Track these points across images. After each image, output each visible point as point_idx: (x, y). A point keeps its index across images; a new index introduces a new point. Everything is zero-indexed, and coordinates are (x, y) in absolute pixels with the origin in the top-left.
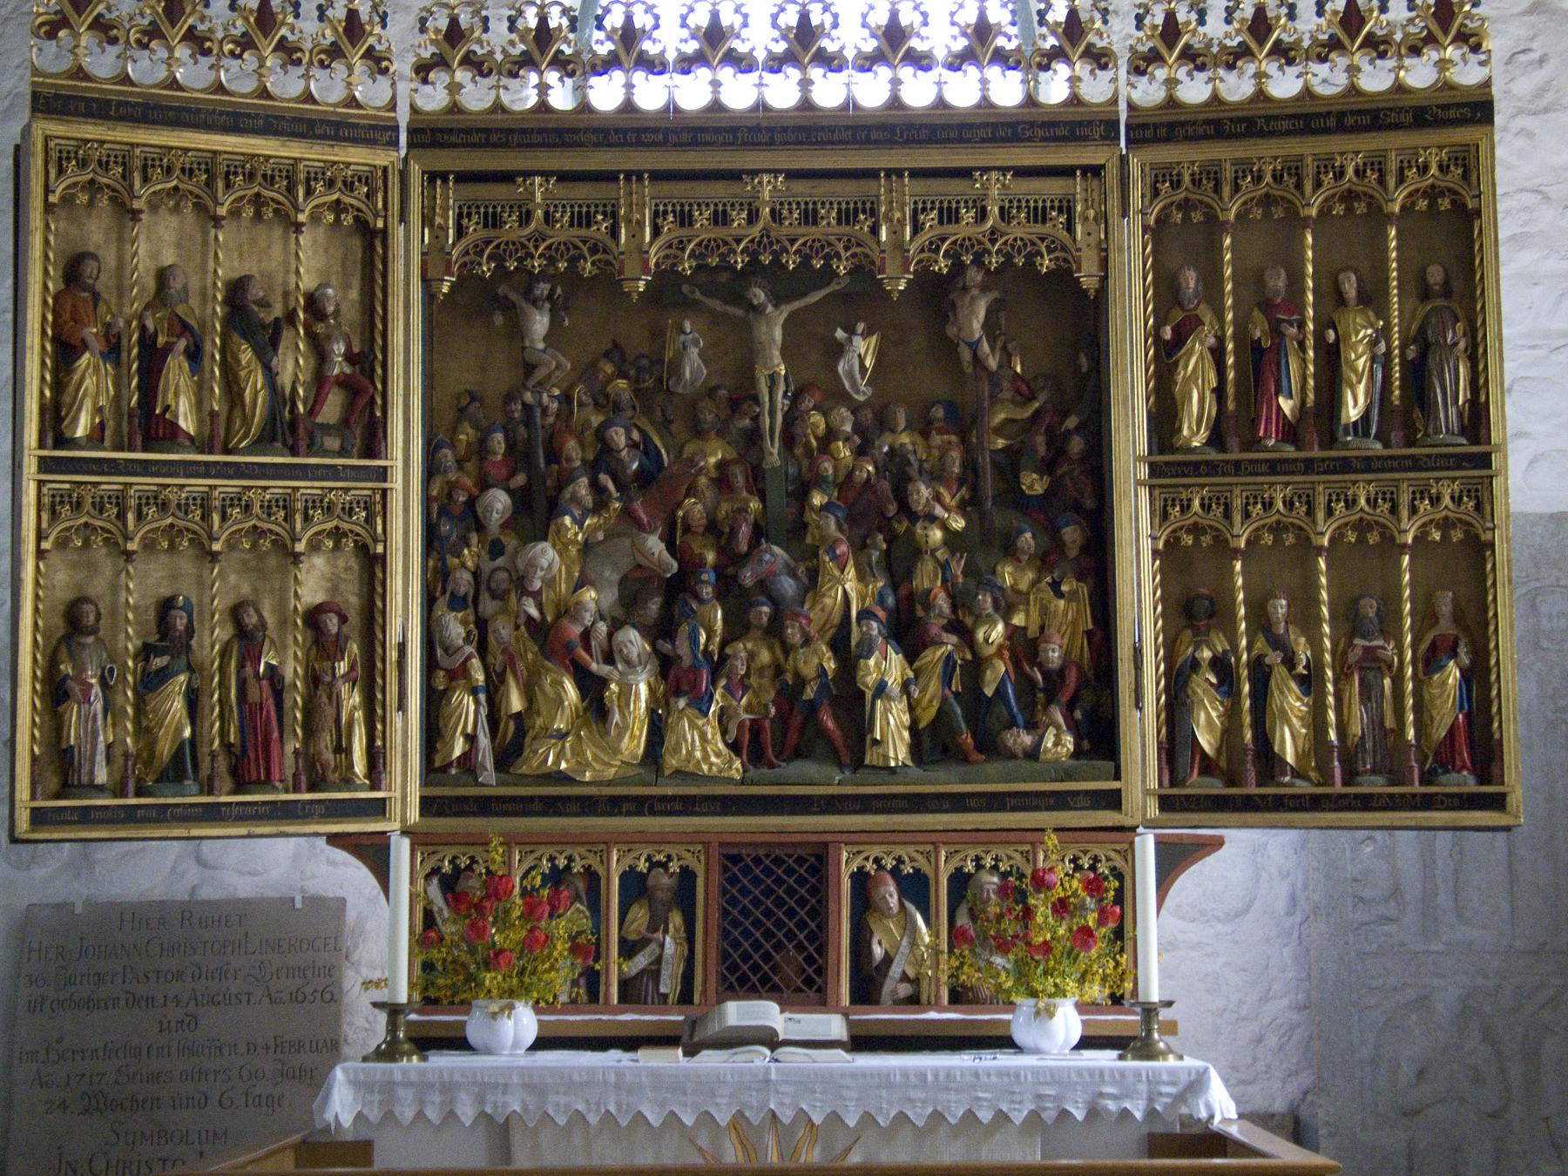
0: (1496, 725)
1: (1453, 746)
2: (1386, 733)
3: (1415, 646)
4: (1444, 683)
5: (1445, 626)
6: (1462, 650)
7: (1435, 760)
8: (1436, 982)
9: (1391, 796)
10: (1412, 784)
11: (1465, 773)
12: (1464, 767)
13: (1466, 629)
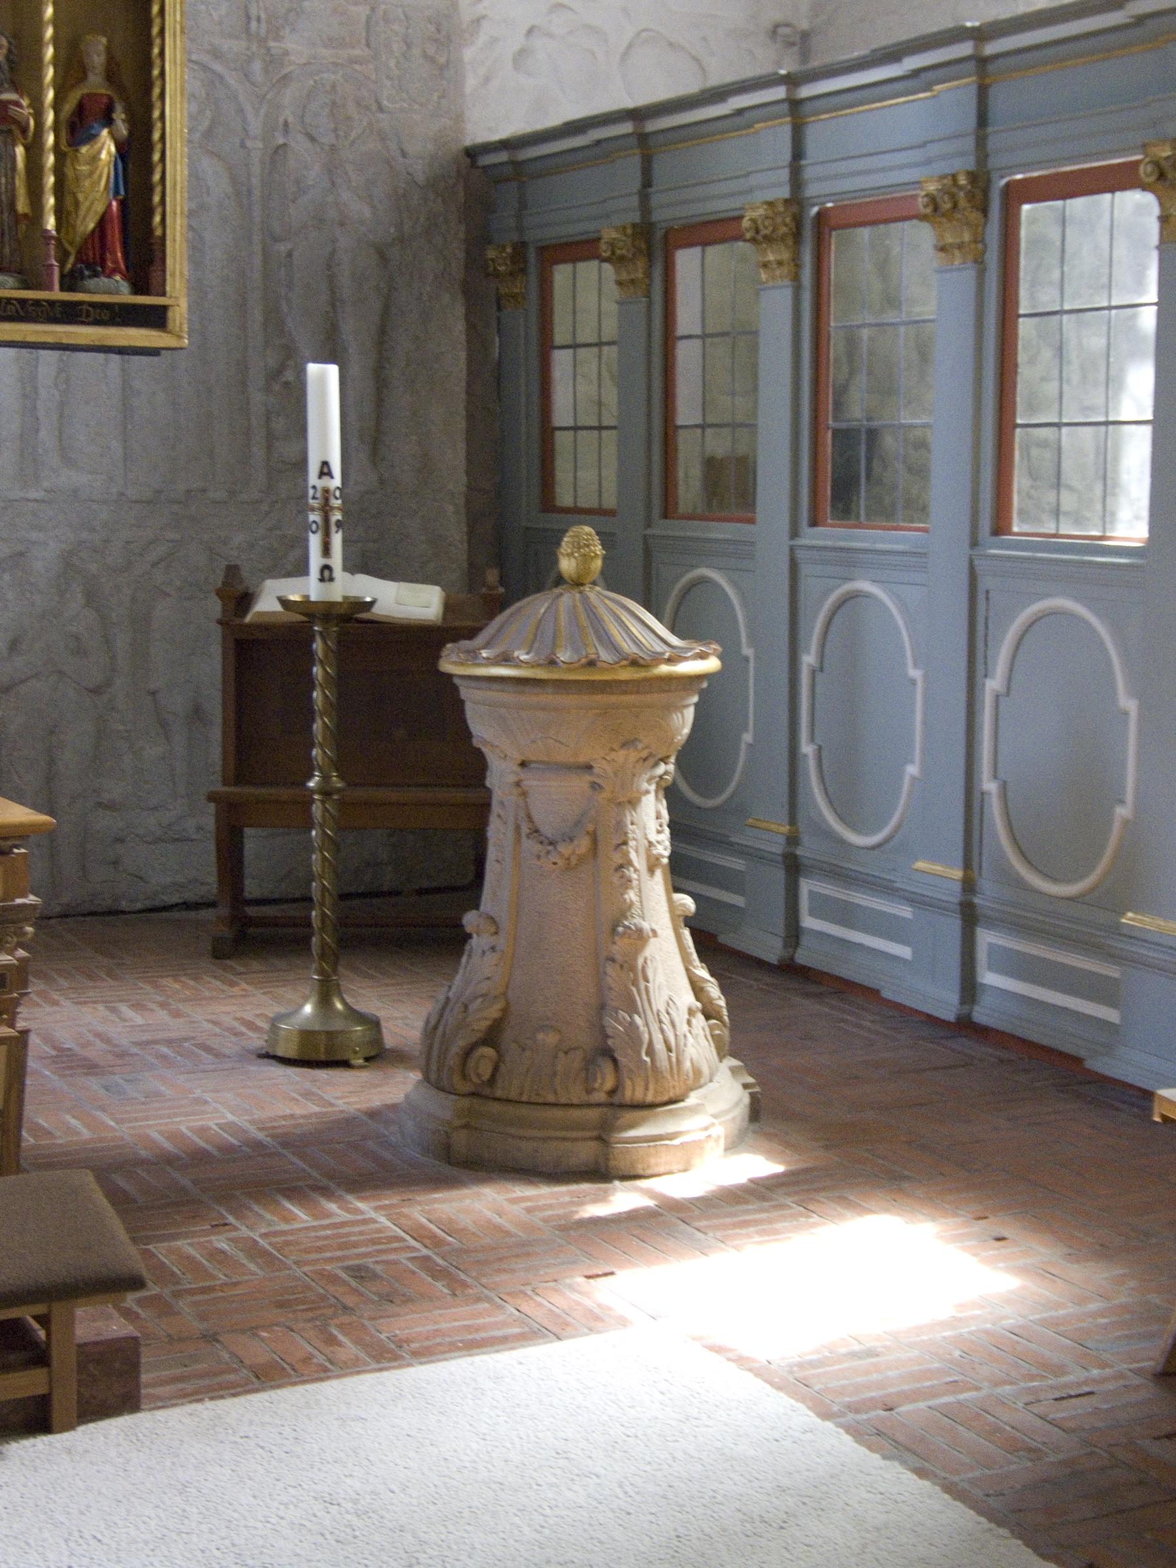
0: (157, 219)
1: (103, 246)
2: (17, 218)
3: (57, 105)
4: (95, 158)
5: (96, 83)
6: (119, 116)
7: (79, 259)
8: (34, 535)
9: (23, 302)
10: (50, 288)
11: (118, 278)
12: (114, 271)
13: (121, 89)
